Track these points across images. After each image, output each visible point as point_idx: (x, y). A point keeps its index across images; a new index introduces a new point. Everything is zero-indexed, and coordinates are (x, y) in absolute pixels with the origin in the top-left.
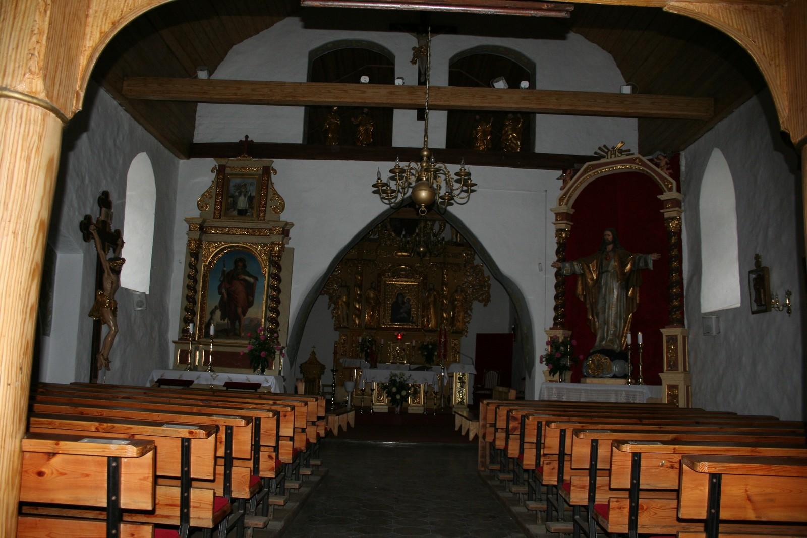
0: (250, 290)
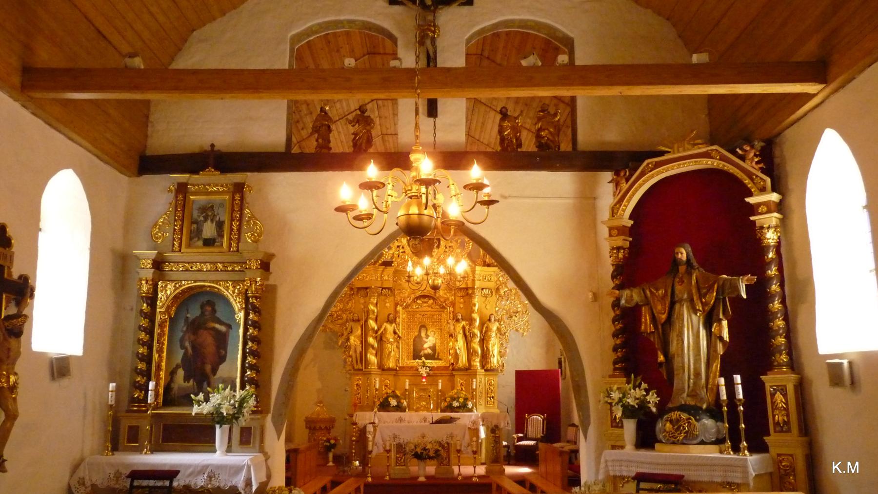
0: (222, 341)
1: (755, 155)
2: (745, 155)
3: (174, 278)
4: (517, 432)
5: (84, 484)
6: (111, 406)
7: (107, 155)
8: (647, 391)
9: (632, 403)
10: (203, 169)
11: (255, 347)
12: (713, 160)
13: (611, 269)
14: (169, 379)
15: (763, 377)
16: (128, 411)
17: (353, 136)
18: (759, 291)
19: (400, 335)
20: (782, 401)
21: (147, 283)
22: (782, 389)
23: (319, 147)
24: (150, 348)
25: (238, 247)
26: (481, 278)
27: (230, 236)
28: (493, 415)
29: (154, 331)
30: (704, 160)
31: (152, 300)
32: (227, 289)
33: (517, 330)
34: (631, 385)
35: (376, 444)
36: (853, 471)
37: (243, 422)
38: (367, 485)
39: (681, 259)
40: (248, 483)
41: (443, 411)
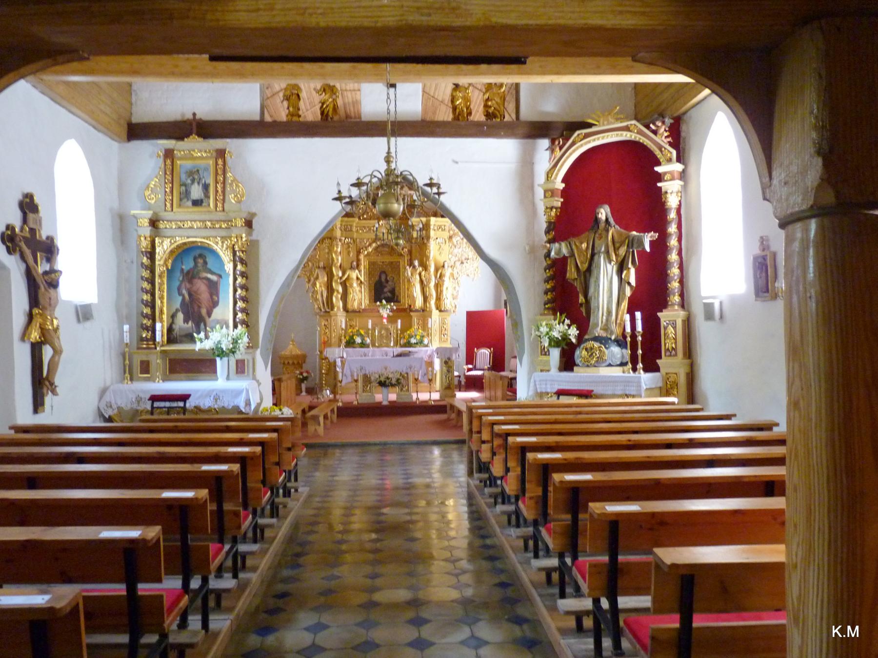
0: (214, 288)
1: (665, 130)
2: (657, 130)
3: (169, 234)
4: (467, 364)
5: (111, 407)
6: (127, 344)
7: (101, 125)
8: (569, 326)
9: (556, 336)
10: (188, 136)
11: (244, 293)
12: (631, 133)
13: (544, 226)
14: (171, 321)
15: (659, 314)
16: (139, 348)
17: (320, 105)
18: (660, 246)
19: (363, 280)
20: (672, 332)
21: (145, 238)
22: (673, 324)
23: (291, 115)
24: (153, 295)
25: (223, 207)
26: (436, 228)
27: (216, 197)
28: (446, 349)
29: (155, 281)
30: (625, 133)
31: (151, 255)
32: (217, 243)
33: (468, 275)
34: (557, 322)
35: (344, 376)
36: (853, 635)
37: (238, 356)
38: (338, 408)
39: (601, 218)
40: (248, 403)
41: (401, 346)
